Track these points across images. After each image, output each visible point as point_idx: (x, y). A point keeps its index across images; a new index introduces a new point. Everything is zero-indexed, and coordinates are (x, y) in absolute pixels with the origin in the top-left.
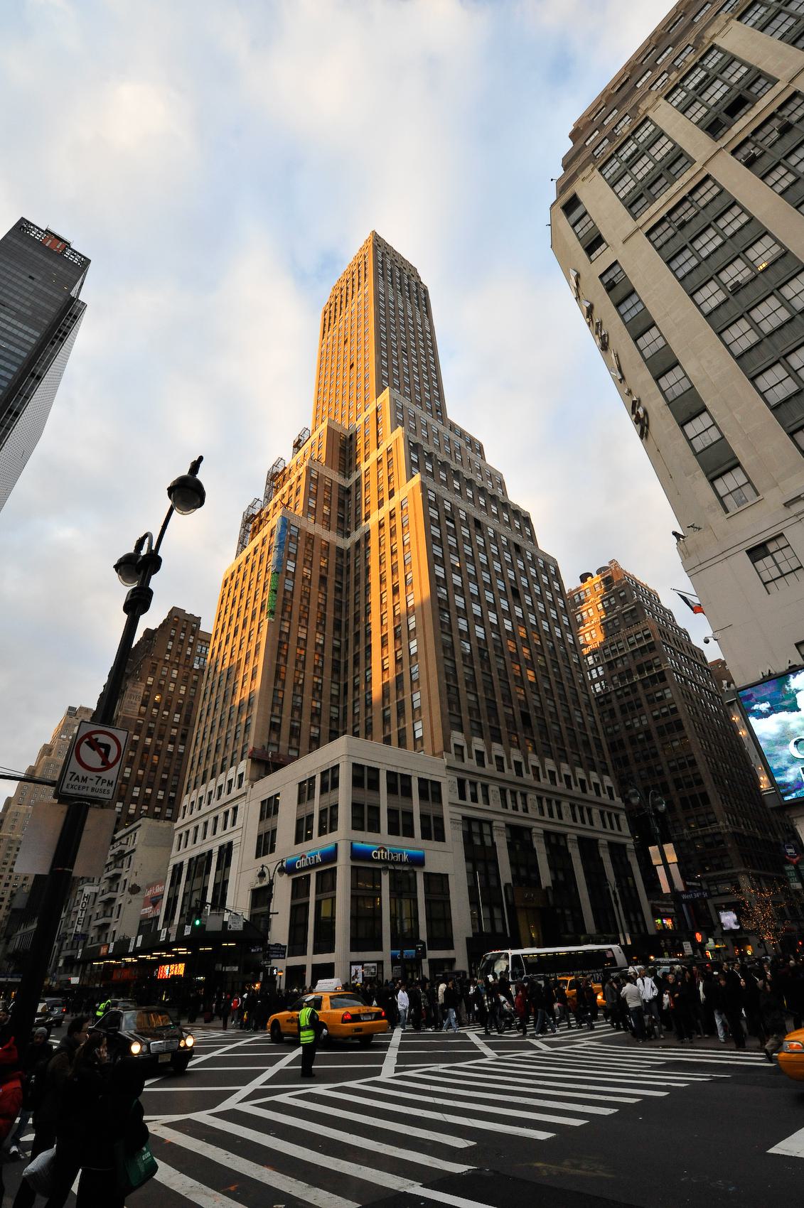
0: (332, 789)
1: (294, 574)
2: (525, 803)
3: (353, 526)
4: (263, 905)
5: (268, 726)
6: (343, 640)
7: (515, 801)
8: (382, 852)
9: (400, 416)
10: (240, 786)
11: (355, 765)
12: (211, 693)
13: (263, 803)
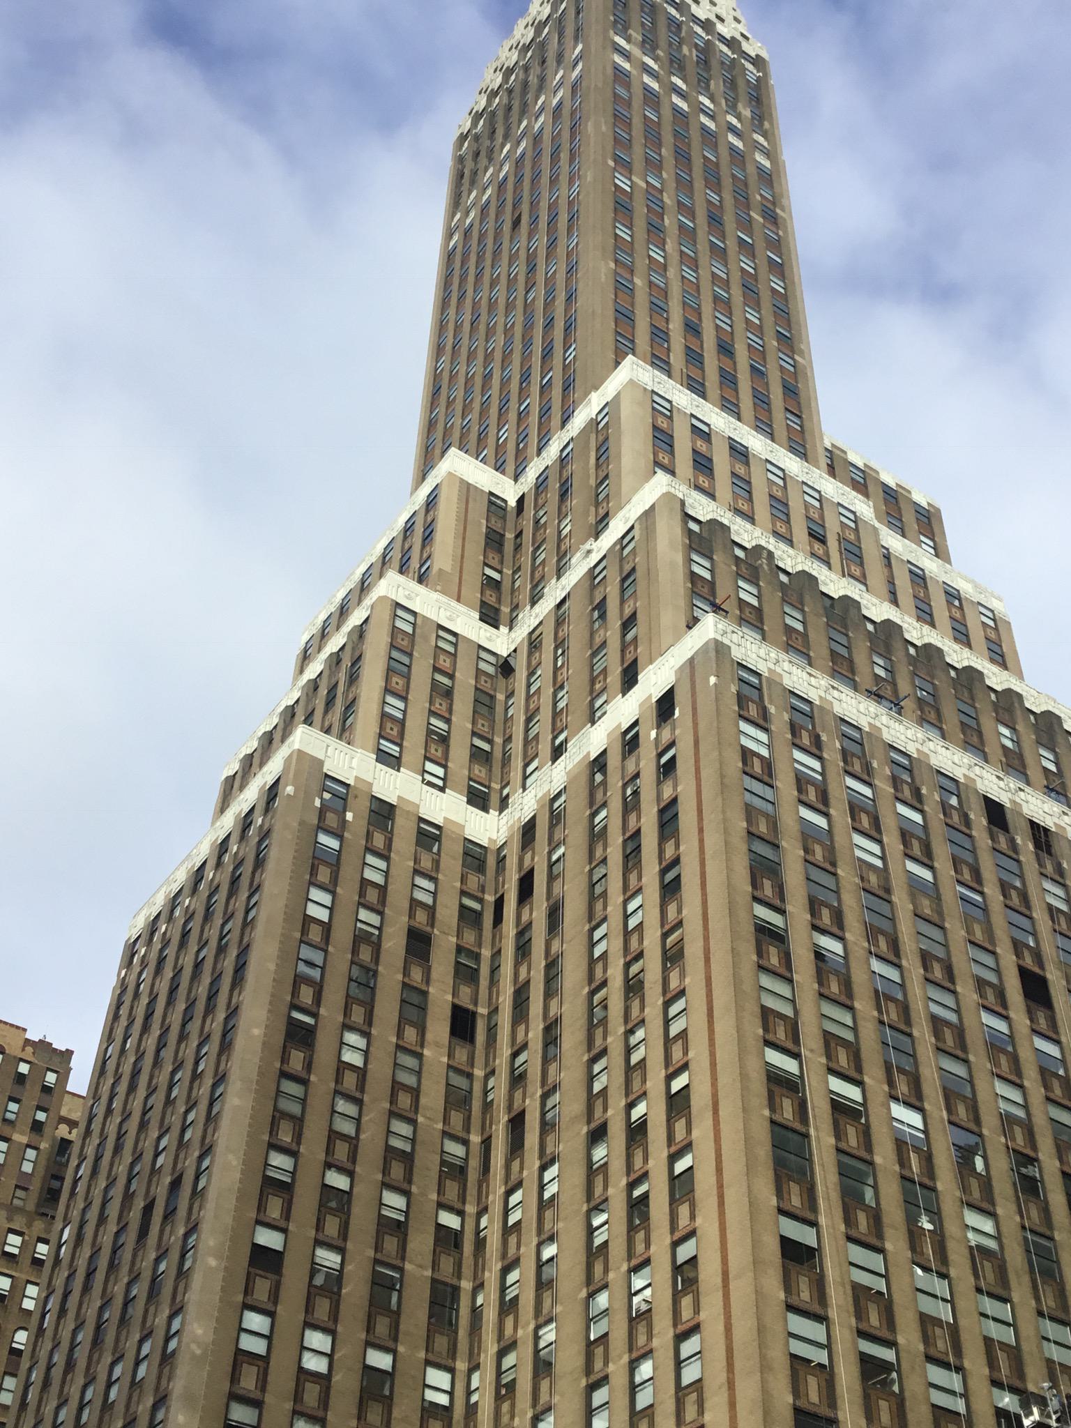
0: (839, 1161)
1: (327, 928)
3: (516, 775)
6: (475, 1139)
12: (87, 1288)
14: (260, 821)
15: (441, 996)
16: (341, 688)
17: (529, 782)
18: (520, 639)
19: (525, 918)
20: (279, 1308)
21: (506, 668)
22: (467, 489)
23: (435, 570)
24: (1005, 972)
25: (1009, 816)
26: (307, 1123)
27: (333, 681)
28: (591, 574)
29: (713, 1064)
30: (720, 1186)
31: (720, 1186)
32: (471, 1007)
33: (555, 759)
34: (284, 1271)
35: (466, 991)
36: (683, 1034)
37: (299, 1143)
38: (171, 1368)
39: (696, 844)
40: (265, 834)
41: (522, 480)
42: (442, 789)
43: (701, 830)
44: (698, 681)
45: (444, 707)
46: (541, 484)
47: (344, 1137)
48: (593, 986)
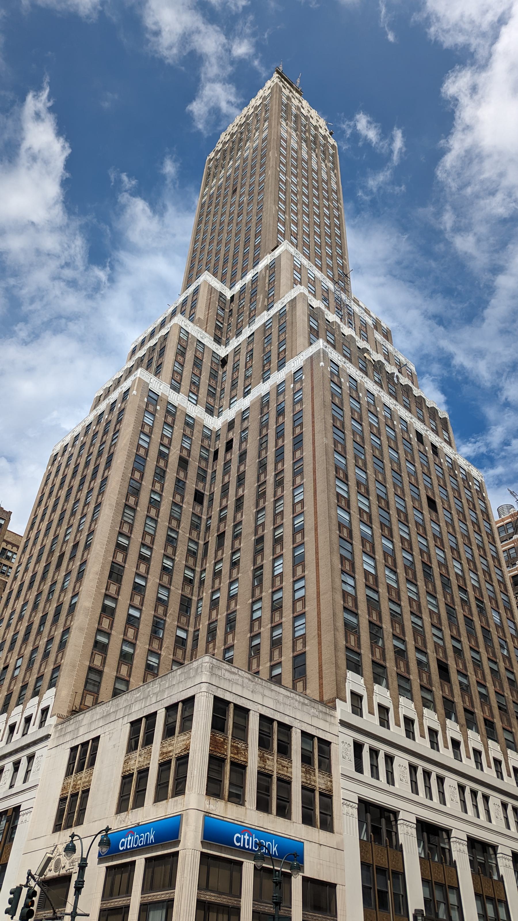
2: (442, 793)
3: (225, 402)
4: (163, 888)
5: (92, 644)
7: (428, 788)
8: (246, 837)
9: (297, 276)
10: (42, 724)
11: (217, 699)
13: (74, 749)
14: (119, 405)
15: (191, 485)
16: (155, 359)
17: (232, 406)
18: (229, 351)
19: (228, 458)
20: (120, 597)
21: (224, 362)
22: (212, 290)
23: (197, 318)
24: (422, 496)
25: (424, 439)
26: (135, 526)
27: (151, 357)
28: (264, 325)
29: (316, 513)
30: (317, 559)
31: (317, 559)
32: (202, 491)
33: (244, 397)
34: (123, 583)
35: (201, 485)
36: (302, 502)
37: (131, 533)
38: (72, 618)
39: (311, 428)
40: (122, 411)
41: (233, 289)
42: (196, 405)
43: (313, 422)
44: (314, 364)
45: (198, 372)
46: (243, 289)
47: (149, 534)
48: (259, 483)
